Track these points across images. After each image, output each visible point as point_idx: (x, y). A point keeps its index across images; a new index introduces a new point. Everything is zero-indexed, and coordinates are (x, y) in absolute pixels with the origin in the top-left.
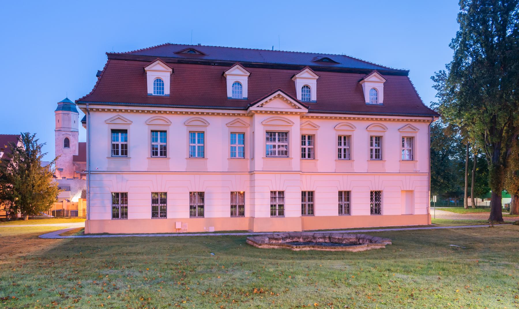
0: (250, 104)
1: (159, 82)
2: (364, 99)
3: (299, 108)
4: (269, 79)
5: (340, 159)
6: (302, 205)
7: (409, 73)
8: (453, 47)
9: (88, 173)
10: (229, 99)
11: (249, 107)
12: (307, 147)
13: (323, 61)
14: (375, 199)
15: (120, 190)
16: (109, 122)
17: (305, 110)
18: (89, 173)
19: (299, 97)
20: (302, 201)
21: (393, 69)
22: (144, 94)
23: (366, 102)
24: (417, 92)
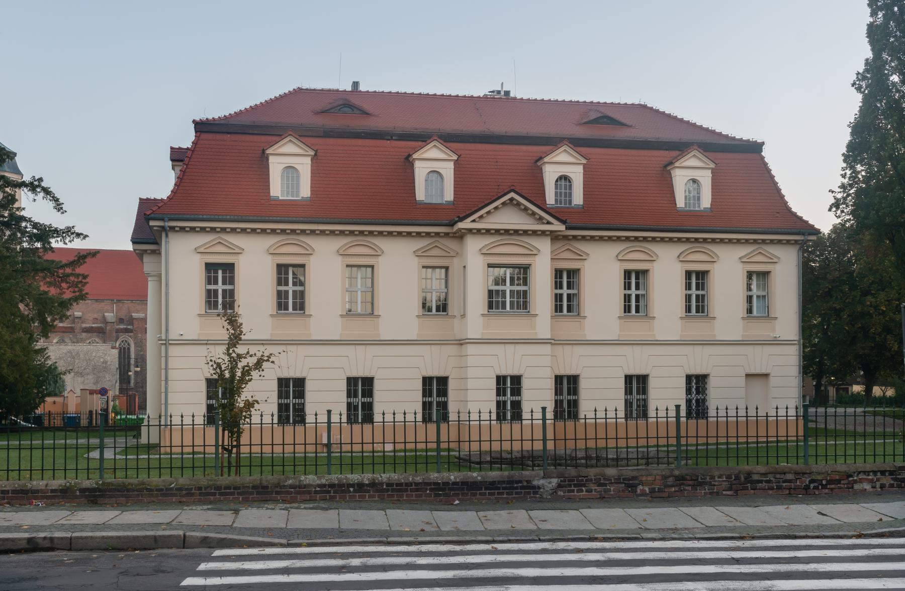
0: (459, 217)
2: (675, 200)
3: (549, 223)
4: (493, 163)
5: (629, 314)
6: (556, 401)
7: (763, 148)
8: (859, 89)
9: (165, 344)
10: (420, 204)
11: (456, 222)
12: (565, 291)
13: (598, 123)
14: (696, 389)
16: (202, 250)
17: (558, 227)
18: (167, 344)
19: (550, 199)
20: (556, 394)
21: (734, 139)
22: (264, 198)
23: (678, 206)
24: (779, 185)
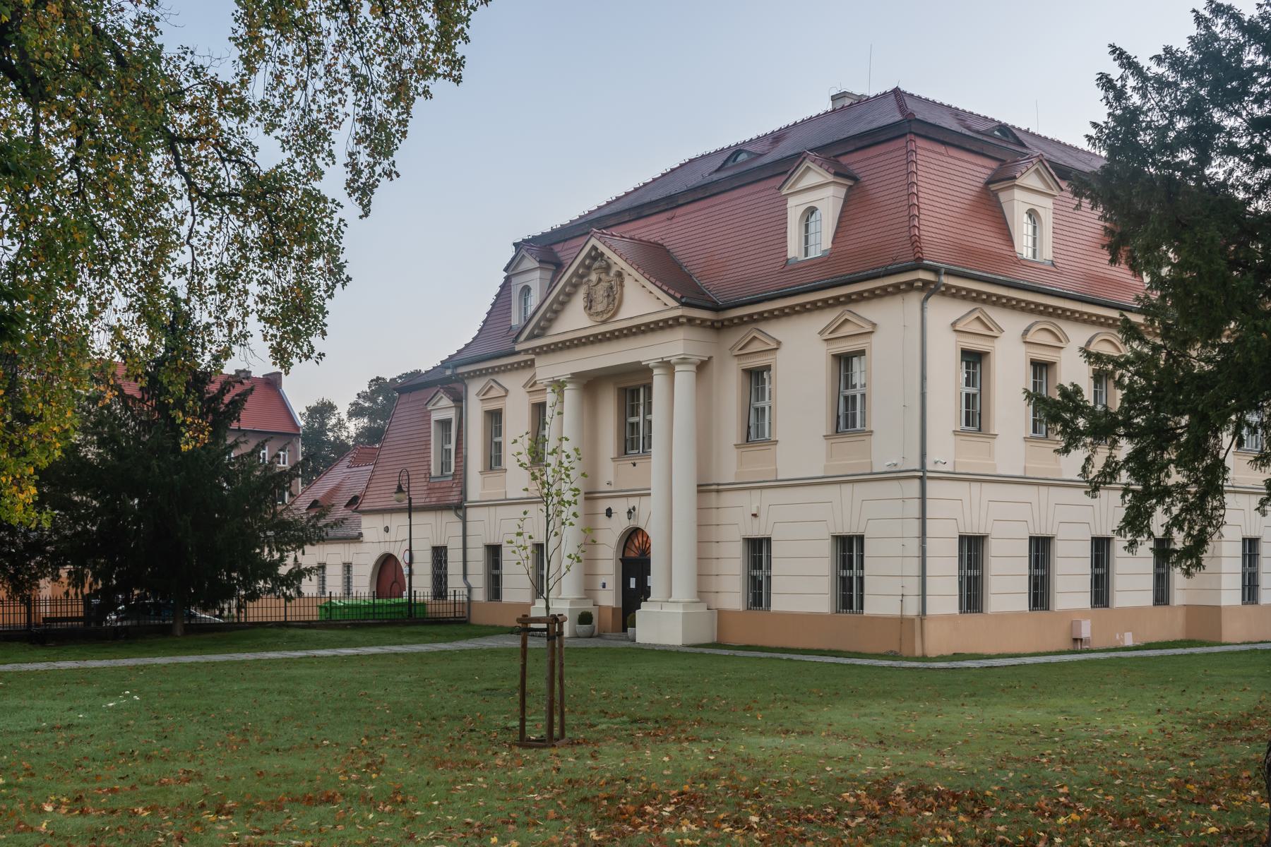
15: (757, 532)
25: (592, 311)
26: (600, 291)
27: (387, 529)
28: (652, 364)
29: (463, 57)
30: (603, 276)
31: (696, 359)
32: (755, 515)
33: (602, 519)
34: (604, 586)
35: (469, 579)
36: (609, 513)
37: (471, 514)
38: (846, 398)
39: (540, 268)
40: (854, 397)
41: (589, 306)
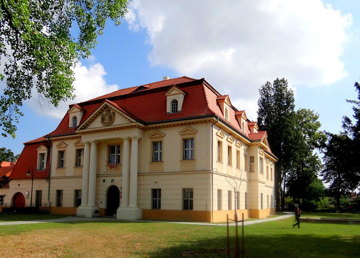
1: (175, 102)
15: (156, 187)
25: (103, 123)
26: (107, 118)
27: (19, 185)
28: (124, 138)
29: (5, 66)
30: (108, 113)
31: (138, 138)
32: (156, 182)
33: (101, 183)
34: (101, 202)
35: (50, 200)
36: (104, 181)
37: (52, 181)
38: (155, 153)
39: (80, 112)
40: (157, 153)
41: (103, 120)
